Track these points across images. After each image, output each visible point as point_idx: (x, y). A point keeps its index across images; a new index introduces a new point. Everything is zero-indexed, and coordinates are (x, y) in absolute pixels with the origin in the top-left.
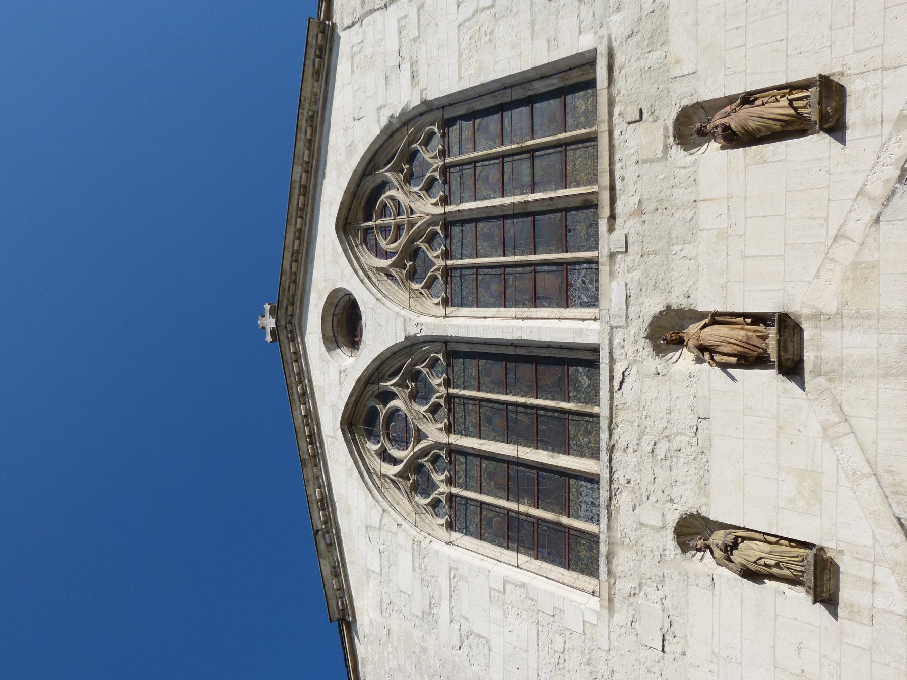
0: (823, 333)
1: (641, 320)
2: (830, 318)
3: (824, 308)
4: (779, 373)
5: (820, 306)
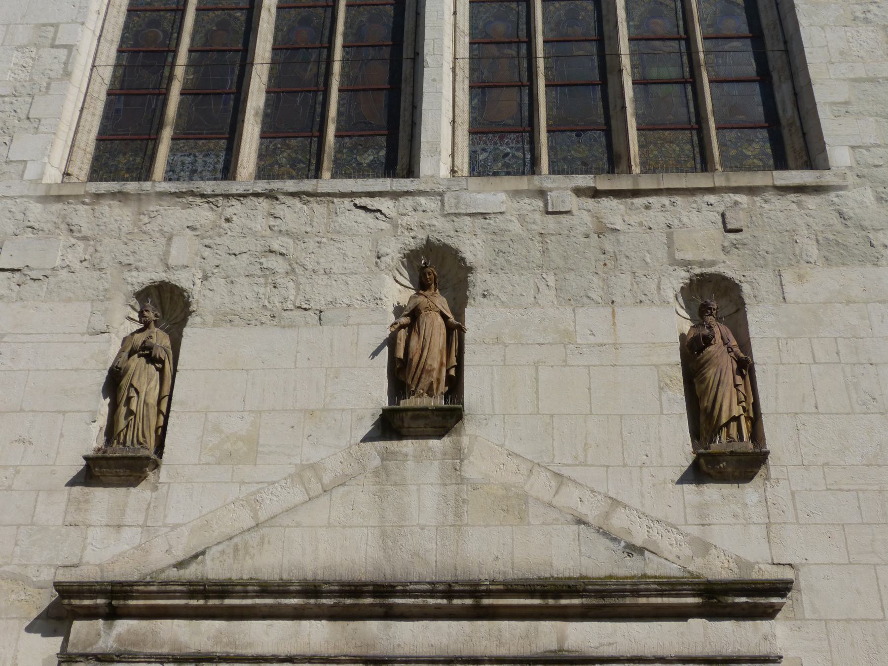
2: (456, 470)
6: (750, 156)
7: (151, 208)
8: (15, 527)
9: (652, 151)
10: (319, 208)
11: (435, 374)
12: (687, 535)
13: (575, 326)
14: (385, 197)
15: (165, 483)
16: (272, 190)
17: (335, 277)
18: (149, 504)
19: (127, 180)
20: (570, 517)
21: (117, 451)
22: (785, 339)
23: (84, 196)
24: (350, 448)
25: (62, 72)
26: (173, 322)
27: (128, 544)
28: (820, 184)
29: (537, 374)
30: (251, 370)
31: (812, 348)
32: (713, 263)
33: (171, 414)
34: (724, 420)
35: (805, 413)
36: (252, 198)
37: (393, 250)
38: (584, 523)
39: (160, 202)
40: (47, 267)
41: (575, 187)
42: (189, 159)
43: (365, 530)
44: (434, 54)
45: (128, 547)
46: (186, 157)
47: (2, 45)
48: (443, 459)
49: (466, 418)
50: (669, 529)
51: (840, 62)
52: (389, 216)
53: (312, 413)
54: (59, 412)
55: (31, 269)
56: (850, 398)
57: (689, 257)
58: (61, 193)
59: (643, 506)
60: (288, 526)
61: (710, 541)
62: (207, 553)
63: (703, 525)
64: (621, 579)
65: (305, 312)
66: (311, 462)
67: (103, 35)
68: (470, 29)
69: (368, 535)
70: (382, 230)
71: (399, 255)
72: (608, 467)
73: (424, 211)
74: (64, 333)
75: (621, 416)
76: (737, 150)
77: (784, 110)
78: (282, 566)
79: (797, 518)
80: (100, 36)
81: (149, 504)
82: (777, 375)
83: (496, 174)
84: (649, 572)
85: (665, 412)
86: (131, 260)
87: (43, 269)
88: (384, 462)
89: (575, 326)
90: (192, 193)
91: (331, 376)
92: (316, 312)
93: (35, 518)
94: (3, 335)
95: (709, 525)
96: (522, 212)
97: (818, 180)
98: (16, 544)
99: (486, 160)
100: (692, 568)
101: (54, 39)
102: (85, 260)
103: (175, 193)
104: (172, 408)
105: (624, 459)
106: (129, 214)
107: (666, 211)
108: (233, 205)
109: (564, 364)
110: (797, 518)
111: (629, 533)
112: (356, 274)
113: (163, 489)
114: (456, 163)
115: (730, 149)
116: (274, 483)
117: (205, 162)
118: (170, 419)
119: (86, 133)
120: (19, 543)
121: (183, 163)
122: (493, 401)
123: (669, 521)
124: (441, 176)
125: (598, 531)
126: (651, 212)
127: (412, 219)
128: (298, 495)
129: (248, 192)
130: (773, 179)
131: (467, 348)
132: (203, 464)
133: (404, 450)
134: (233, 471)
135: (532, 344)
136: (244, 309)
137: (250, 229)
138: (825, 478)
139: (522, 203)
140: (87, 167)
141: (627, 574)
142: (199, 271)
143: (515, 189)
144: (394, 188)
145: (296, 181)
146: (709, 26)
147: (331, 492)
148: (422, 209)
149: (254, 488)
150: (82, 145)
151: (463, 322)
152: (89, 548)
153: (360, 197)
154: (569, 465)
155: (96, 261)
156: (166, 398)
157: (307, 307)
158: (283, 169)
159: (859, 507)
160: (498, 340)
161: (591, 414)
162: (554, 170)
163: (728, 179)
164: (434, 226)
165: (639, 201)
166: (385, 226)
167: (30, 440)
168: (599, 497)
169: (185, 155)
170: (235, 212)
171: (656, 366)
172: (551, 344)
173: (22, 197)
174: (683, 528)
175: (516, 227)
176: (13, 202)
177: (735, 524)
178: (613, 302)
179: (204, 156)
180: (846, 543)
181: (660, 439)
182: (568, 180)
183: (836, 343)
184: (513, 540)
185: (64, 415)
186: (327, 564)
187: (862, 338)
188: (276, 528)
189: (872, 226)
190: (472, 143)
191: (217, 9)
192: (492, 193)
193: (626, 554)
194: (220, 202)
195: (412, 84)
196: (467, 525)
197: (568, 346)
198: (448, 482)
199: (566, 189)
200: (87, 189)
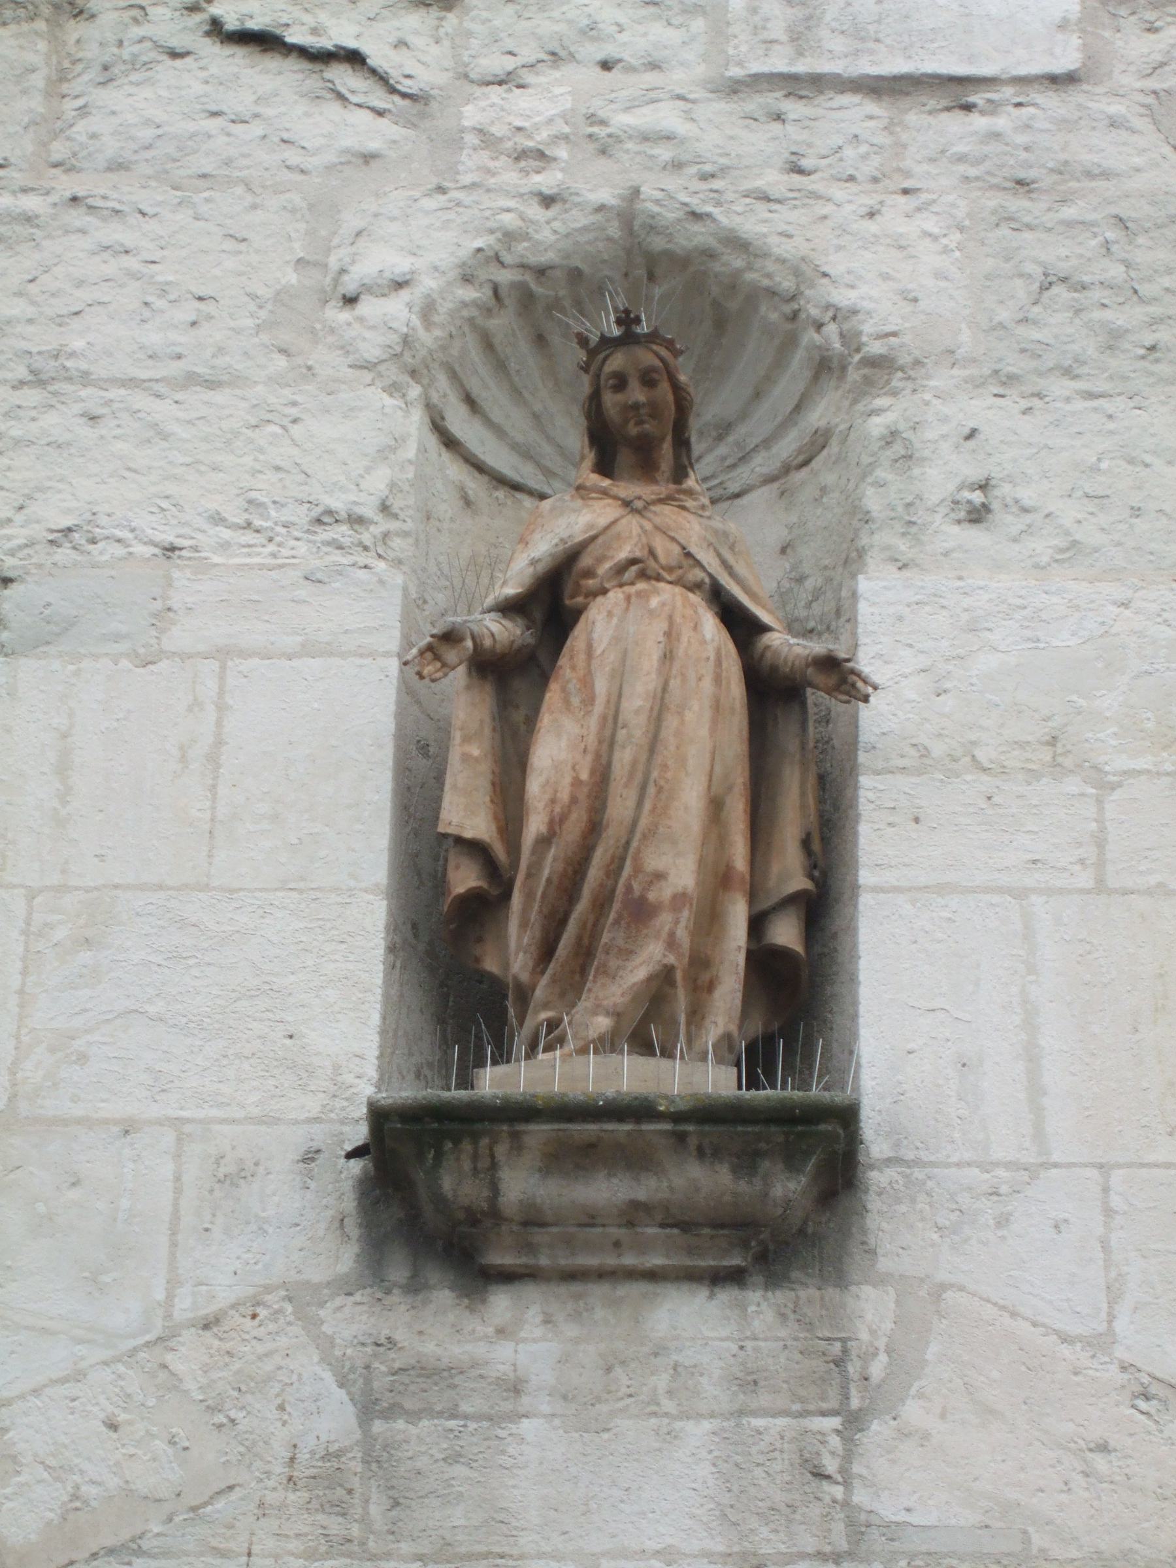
0: (698, 1432)
1: (773, 179)
2: (820, 1475)
3: (904, 1434)
4: (379, 1116)
5: (913, 1412)
11: (682, 926)
17: (91, 397)
48: (741, 1413)
49: (877, 1179)
52: (406, 86)
71: (469, 294)
73: (606, 66)
88: (378, 1426)
91: (60, 934)
112: (212, 384)
122: (1035, 1090)
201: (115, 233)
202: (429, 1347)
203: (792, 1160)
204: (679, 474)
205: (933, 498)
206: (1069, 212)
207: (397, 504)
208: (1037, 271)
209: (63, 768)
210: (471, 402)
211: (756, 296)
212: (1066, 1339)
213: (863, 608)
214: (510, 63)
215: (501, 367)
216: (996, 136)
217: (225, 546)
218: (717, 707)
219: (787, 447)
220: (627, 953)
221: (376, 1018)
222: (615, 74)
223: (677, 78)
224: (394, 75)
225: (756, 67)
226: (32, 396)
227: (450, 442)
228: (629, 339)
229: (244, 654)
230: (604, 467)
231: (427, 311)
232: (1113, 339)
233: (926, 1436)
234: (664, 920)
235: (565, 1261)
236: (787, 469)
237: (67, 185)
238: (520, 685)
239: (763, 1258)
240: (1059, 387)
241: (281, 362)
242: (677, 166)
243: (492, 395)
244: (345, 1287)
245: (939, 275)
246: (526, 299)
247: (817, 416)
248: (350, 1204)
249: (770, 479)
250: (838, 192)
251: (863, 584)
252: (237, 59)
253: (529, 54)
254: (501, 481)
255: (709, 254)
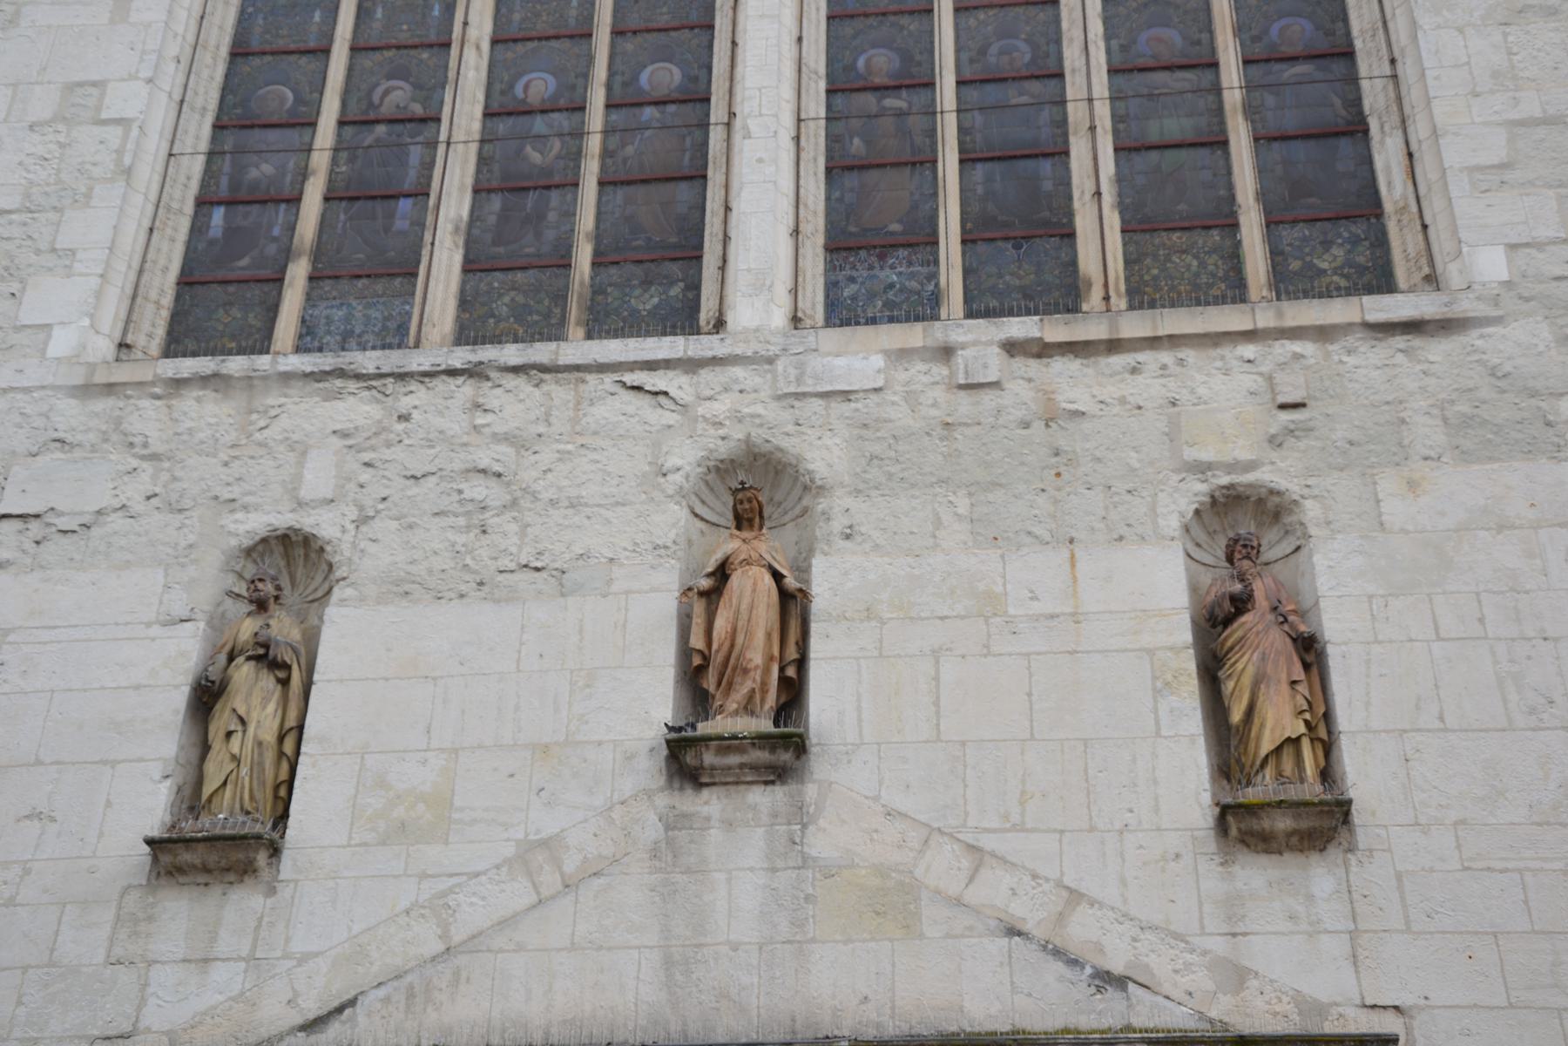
0: (760, 831)
1: (790, 428)
2: (795, 843)
5: (821, 822)
6: (1325, 271)
7: (271, 401)
8: (19, 972)
9: (1149, 269)
10: (559, 392)
11: (758, 676)
12: (1205, 953)
13: (1004, 585)
14: (675, 369)
15: (288, 881)
16: (481, 363)
17: (588, 511)
18: (260, 920)
19: (230, 353)
20: (993, 923)
21: (205, 825)
22: (1382, 596)
23: (153, 384)
24: (610, 809)
25: (112, 167)
26: (310, 598)
27: (221, 993)
28: (1450, 315)
29: (937, 671)
30: (442, 677)
31: (1433, 613)
32: (1251, 466)
33: (301, 759)
34: (1266, 746)
35: (1419, 730)
36: (444, 377)
37: (686, 457)
38: (1020, 934)
39: (285, 390)
40: (87, 508)
41: (1007, 339)
42: (339, 314)
43: (635, 953)
44: (761, 115)
45: (221, 998)
46: (334, 310)
47: (5, 120)
48: (772, 825)
49: (814, 750)
50: (1173, 942)
51: (1492, 92)
52: (681, 402)
53: (546, 749)
54: (104, 762)
55: (61, 514)
56: (1505, 701)
57: (1206, 455)
58: (113, 380)
59: (1125, 901)
60: (501, 951)
61: (1247, 963)
62: (359, 1002)
63: (1234, 935)
64: (1084, 1033)
65: (537, 574)
66: (544, 835)
67: (187, 99)
68: (827, 66)
69: (640, 963)
70: (540, 436)
71: (700, 470)
72: (1062, 832)
73: (741, 392)
74: (117, 624)
75: (1085, 741)
76: (1303, 259)
77: (1389, 184)
78: (489, 1021)
79: (1408, 923)
80: (182, 102)
81: (260, 920)
82: (1368, 662)
83: (873, 321)
84: (1137, 1022)
85: (1164, 732)
86: (235, 491)
87: (82, 513)
88: (670, 833)
89: (1004, 585)
90: (340, 373)
91: (580, 684)
92: (554, 573)
93: (55, 953)
94: (7, 632)
95: (1245, 934)
96: (913, 387)
97: (1446, 309)
98: (19, 1003)
99: (854, 298)
100: (1213, 1014)
101: (98, 109)
102: (156, 495)
103: (312, 373)
104: (303, 749)
105: (1091, 818)
106: (232, 412)
107: (1170, 376)
108: (411, 392)
109: (985, 651)
110: (1408, 923)
111: (1100, 949)
112: (624, 505)
113: (285, 892)
114: (800, 304)
115: (1290, 260)
116: (477, 875)
117: (367, 317)
118: (299, 767)
119: (159, 273)
120: (24, 999)
121: (329, 319)
122: (860, 720)
123: (1172, 928)
124: (773, 326)
125: (1045, 948)
126: (1139, 378)
127: (720, 408)
128: (518, 895)
129: (439, 369)
130: (1362, 310)
131: (814, 628)
132: (356, 845)
133: (705, 810)
134: (408, 855)
135: (928, 618)
136: (430, 572)
137: (441, 432)
138: (1459, 847)
139: (913, 371)
140: (161, 332)
141: (1095, 1025)
142: (353, 508)
143: (899, 346)
144: (690, 353)
145: (520, 346)
146: (1256, 39)
147: (577, 887)
148: (737, 387)
149: (444, 884)
150: (153, 295)
151: (808, 582)
152: (152, 1001)
153: (632, 370)
154: (994, 831)
155: (174, 497)
156: (293, 733)
157: (539, 564)
158: (502, 325)
159: (1526, 902)
160: (869, 613)
161: (1032, 738)
162: (973, 311)
163: (1280, 314)
164: (759, 416)
165: (1118, 361)
166: (671, 418)
167: (52, 814)
168: (1046, 887)
169: (332, 307)
170: (417, 403)
171: (1151, 652)
172: (962, 618)
173: (43, 387)
174: (1196, 940)
175: (900, 415)
176: (26, 398)
177: (1292, 933)
178: (1071, 541)
179: (365, 308)
180: (1502, 970)
181: (1155, 782)
182: (993, 329)
183: (1479, 602)
184: (893, 965)
185: (113, 767)
186: (570, 1017)
187: (1527, 592)
188: (480, 954)
189: (1547, 388)
190: (830, 268)
191: (388, 47)
192: (861, 355)
193: (1093, 989)
194: (390, 387)
195: (724, 170)
196: (813, 940)
197: (992, 620)
198: (780, 864)
199: (989, 343)
200: (159, 371)
201: (595, 456)
202: (685, 808)
203: (786, 749)
204: (761, 528)
205: (835, 532)
206: (879, 434)
207: (678, 541)
208: (868, 454)
209: (581, 631)
210: (703, 502)
211: (786, 465)
212: (867, 798)
213: (814, 569)
214: (712, 392)
215: (712, 490)
216: (857, 410)
217: (627, 558)
218: (768, 606)
219: (797, 510)
220: (742, 684)
221: (671, 706)
222: (744, 395)
223: (762, 394)
224: (678, 398)
225: (786, 391)
226: (571, 511)
227: (696, 515)
228: (744, 489)
229: (634, 592)
230: (739, 528)
231: (687, 477)
232: (890, 476)
233: (825, 830)
234: (752, 673)
235: (723, 780)
236: (797, 517)
237: (580, 440)
238: (714, 597)
239: (779, 776)
240: (874, 493)
241: (644, 496)
242: (761, 425)
243: (709, 498)
244: (662, 790)
245: (839, 457)
246: (718, 469)
247: (805, 502)
248: (663, 764)
249: (793, 520)
250: (809, 432)
251: (814, 562)
252: (632, 393)
253: (718, 389)
254: (714, 524)
255: (772, 453)
